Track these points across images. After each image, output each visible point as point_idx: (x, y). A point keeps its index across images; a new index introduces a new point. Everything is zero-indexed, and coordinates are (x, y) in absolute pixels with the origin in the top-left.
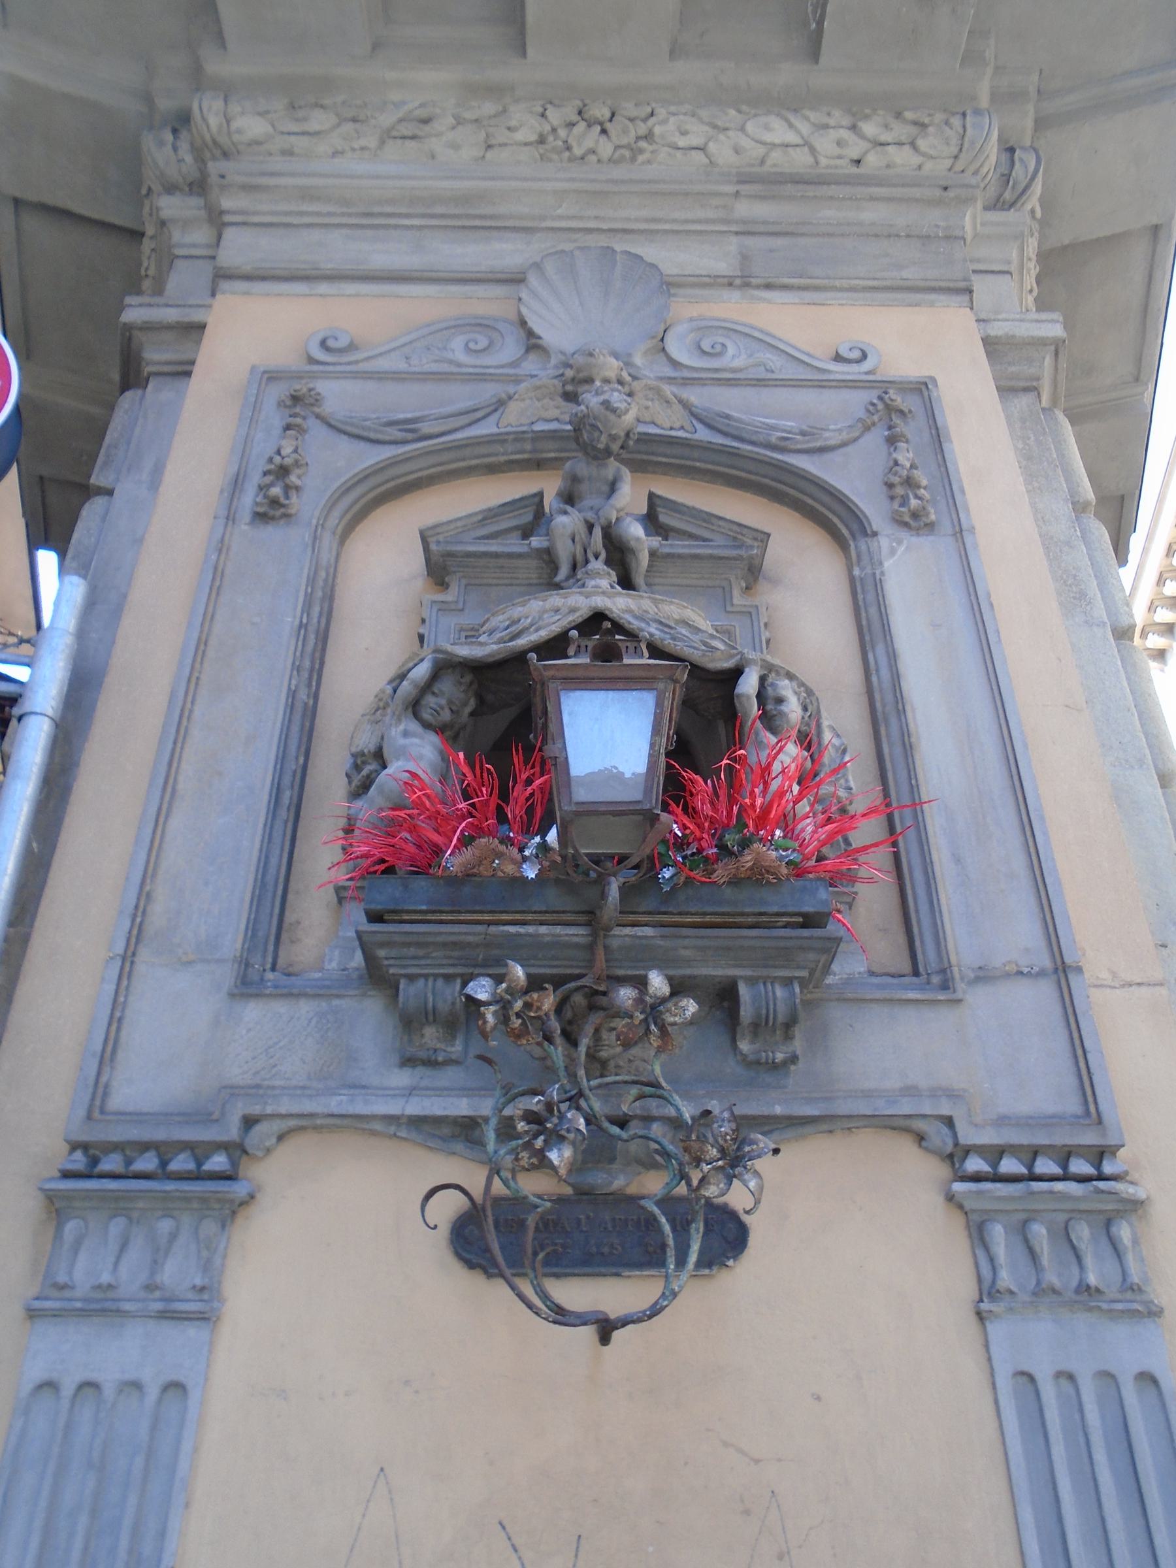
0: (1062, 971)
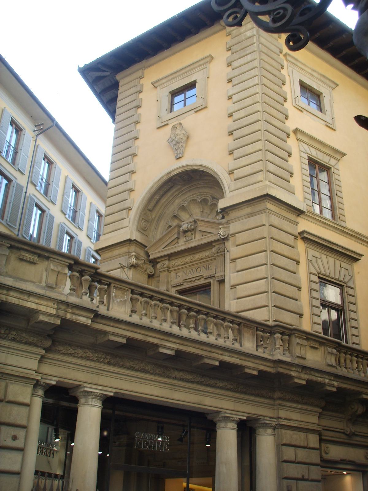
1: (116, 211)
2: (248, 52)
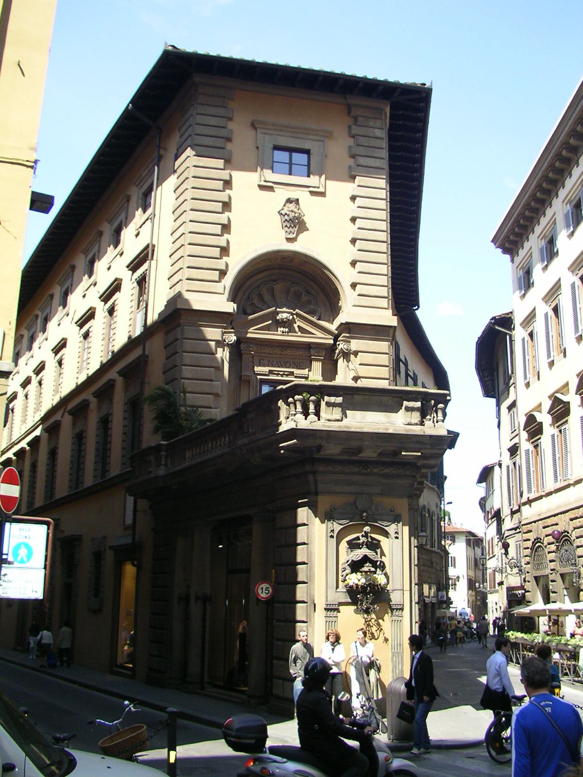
0: (403, 590)
1: (205, 267)
2: (376, 155)
